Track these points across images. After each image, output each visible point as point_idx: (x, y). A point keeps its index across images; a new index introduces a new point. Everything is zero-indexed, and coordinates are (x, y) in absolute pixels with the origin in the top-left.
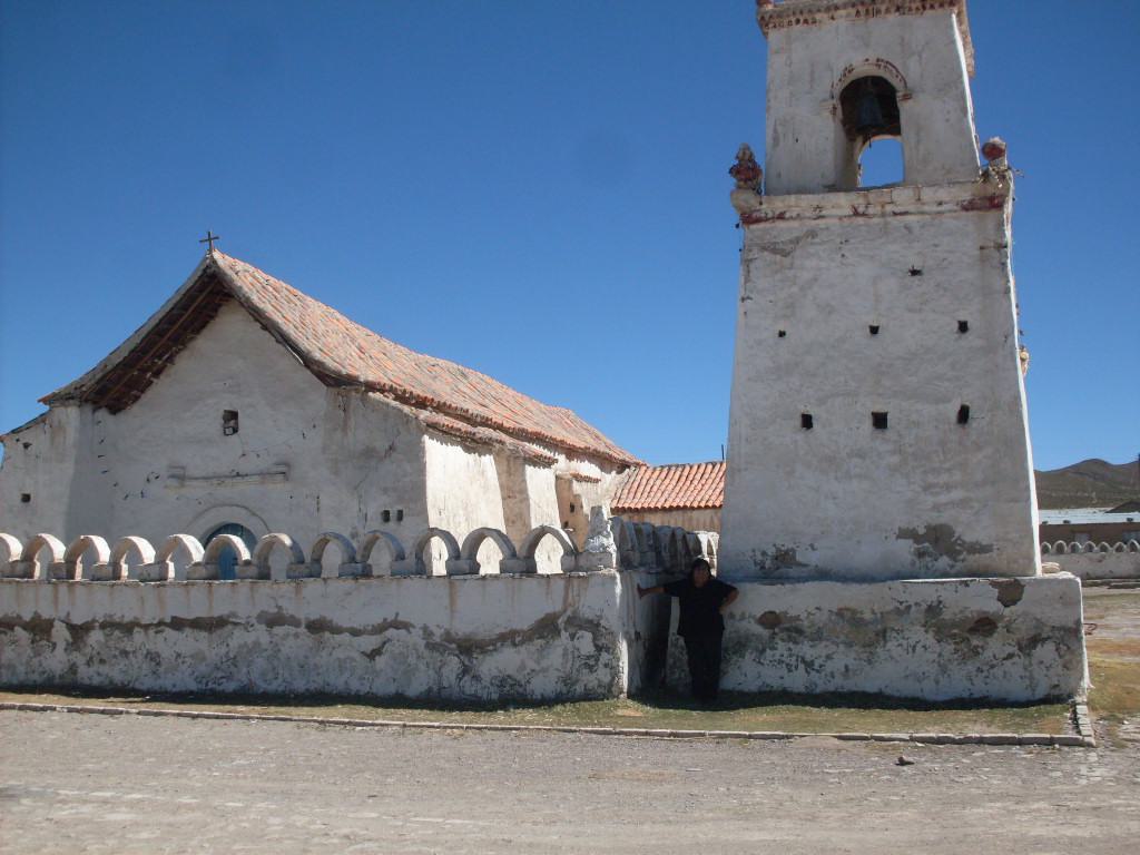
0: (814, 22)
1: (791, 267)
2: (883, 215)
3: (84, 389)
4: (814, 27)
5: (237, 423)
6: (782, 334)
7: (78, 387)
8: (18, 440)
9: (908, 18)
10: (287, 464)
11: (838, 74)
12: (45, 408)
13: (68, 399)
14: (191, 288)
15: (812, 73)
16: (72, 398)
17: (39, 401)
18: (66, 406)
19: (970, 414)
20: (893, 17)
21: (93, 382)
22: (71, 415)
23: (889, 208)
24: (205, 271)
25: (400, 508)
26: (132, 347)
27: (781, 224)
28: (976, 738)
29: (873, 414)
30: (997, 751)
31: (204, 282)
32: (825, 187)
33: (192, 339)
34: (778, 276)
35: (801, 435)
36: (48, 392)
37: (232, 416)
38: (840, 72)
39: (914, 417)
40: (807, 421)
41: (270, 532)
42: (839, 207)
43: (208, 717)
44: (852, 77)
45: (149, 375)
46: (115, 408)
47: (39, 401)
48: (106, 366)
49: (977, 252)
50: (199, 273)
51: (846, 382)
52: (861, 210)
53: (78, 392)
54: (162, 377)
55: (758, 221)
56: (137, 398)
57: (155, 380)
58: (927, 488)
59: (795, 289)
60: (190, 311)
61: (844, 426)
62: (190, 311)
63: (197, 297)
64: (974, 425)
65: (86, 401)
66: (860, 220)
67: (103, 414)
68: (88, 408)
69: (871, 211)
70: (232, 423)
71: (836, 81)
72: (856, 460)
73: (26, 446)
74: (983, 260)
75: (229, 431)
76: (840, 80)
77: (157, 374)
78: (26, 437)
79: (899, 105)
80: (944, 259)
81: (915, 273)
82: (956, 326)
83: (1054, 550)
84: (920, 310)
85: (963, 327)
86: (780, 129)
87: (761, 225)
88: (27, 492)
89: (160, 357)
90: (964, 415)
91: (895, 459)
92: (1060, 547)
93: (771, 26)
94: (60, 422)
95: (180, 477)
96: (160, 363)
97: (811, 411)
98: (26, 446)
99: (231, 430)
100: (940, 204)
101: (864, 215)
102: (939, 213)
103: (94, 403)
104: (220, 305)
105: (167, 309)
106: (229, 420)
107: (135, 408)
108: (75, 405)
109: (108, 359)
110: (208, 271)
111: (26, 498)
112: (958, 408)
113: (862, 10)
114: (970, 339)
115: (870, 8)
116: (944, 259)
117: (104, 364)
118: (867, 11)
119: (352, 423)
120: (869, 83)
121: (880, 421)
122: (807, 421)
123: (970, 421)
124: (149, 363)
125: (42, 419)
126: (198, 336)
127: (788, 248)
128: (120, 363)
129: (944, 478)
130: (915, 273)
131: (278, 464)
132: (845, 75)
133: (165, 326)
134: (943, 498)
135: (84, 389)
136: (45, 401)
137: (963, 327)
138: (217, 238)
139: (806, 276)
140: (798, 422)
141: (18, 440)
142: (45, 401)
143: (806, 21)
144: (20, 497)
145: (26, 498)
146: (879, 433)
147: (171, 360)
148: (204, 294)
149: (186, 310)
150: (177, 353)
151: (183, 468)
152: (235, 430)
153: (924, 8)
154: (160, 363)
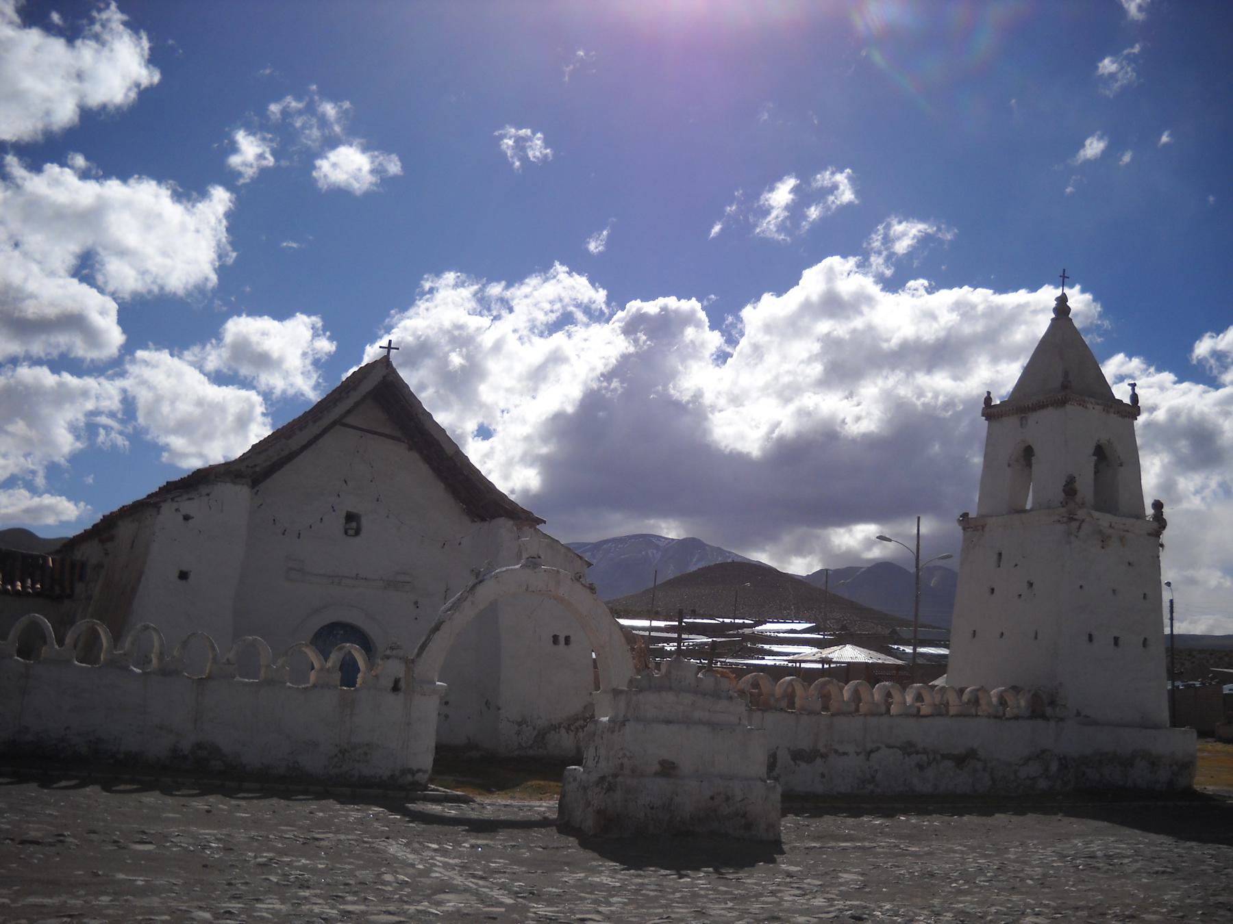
3: (257, 469)
8: (177, 510)
24: (384, 377)
73: (187, 518)
88: (185, 569)
111: (183, 576)
122: (1090, 638)
135: (257, 469)
141: (177, 510)
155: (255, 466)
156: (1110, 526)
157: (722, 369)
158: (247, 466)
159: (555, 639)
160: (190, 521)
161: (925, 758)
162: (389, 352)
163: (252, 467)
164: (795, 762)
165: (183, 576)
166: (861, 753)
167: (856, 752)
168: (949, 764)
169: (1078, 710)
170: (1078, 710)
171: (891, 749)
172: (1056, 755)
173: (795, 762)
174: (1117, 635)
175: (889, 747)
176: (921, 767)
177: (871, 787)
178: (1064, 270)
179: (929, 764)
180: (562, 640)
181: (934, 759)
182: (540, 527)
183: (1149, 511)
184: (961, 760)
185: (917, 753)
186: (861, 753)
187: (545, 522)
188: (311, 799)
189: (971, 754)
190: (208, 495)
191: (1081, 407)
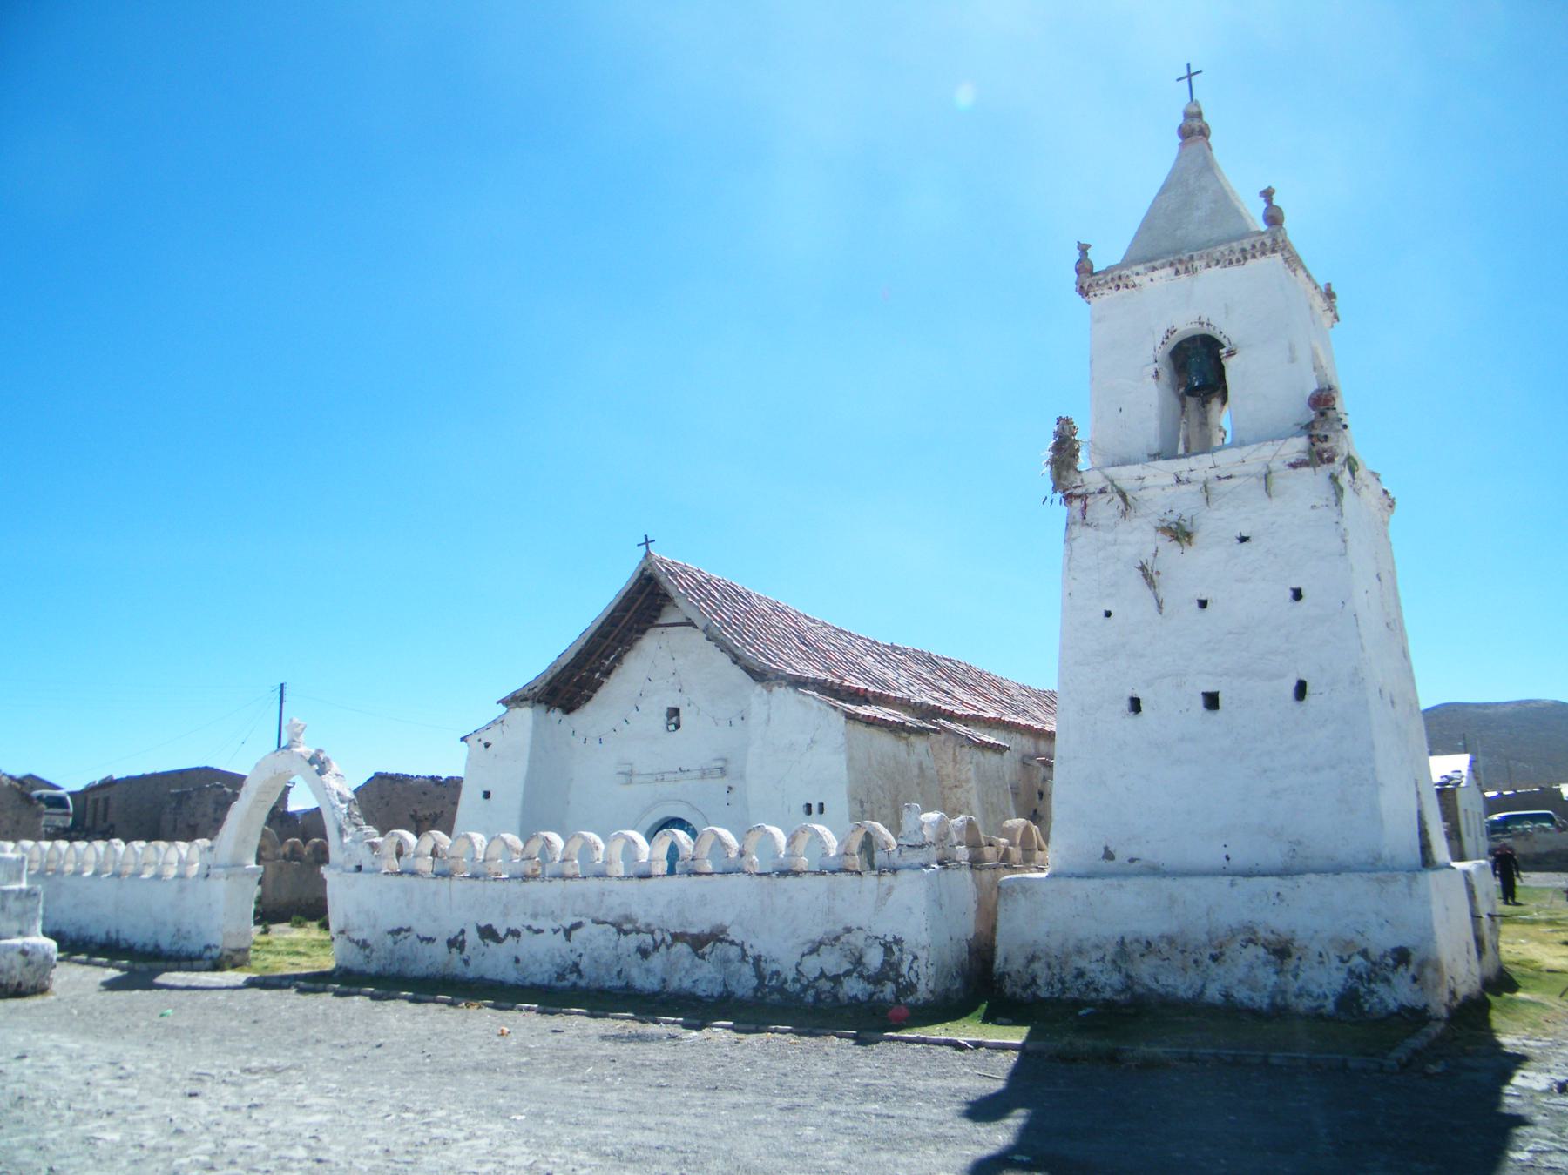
1: (1115, 543)
3: (536, 690)
5: (679, 720)
6: (1108, 614)
7: (530, 687)
8: (480, 740)
10: (725, 760)
11: (1159, 338)
12: (502, 709)
13: (522, 700)
14: (629, 591)
16: (526, 699)
17: (498, 703)
18: (520, 707)
19: (1308, 689)
21: (544, 683)
22: (525, 714)
24: (642, 573)
26: (578, 648)
29: (1203, 693)
30: (933, 1037)
31: (641, 584)
32: (1150, 456)
33: (637, 639)
34: (1101, 554)
35: (1131, 720)
36: (506, 693)
37: (674, 712)
38: (1163, 334)
40: (1136, 705)
41: (709, 825)
44: (1174, 340)
45: (598, 675)
46: (569, 709)
47: (498, 703)
51: (1174, 661)
52: (1183, 477)
53: (531, 693)
54: (612, 676)
56: (589, 698)
57: (605, 680)
60: (631, 612)
62: (631, 612)
63: (637, 599)
65: (539, 702)
66: (1183, 488)
67: (557, 714)
68: (541, 708)
70: (674, 720)
71: (1158, 344)
73: (487, 745)
75: (672, 727)
76: (1163, 343)
77: (607, 673)
79: (1223, 362)
80: (1272, 524)
82: (1289, 594)
88: (487, 789)
89: (607, 658)
90: (1301, 690)
93: (1091, 294)
95: (629, 776)
96: (607, 663)
99: (673, 726)
103: (546, 703)
104: (663, 606)
105: (609, 612)
106: (671, 718)
107: (589, 707)
108: (527, 705)
109: (557, 661)
110: (645, 573)
111: (487, 795)
112: (1294, 683)
113: (1181, 268)
115: (1190, 265)
116: (1272, 524)
117: (553, 666)
118: (1187, 268)
120: (1198, 343)
122: (1136, 705)
123: (1307, 697)
124: (597, 664)
125: (500, 721)
126: (644, 637)
128: (567, 665)
130: (1243, 540)
131: (715, 760)
132: (1167, 338)
133: (608, 628)
135: (536, 690)
136: (504, 702)
138: (654, 541)
140: (1126, 705)
142: (504, 702)
146: (1210, 714)
147: (619, 659)
148: (644, 595)
149: (628, 611)
150: (625, 652)
151: (631, 764)
152: (678, 727)
153: (1246, 259)
154: (607, 663)
155: (535, 688)
156: (1179, 481)
157: (1052, 436)
158: (529, 690)
161: (648, 938)
162: (647, 547)
163: (533, 689)
164: (484, 942)
165: (487, 795)
166: (558, 930)
167: (553, 930)
168: (683, 948)
169: (1106, 849)
170: (1106, 849)
171: (601, 926)
172: (877, 938)
173: (484, 942)
174: (1210, 689)
175: (597, 922)
176: (644, 953)
177: (573, 977)
178: (1200, 71)
179: (656, 948)
181: (663, 940)
184: (698, 943)
185: (638, 931)
186: (558, 930)
188: (790, 1031)
189: (716, 936)
191: (1123, 291)
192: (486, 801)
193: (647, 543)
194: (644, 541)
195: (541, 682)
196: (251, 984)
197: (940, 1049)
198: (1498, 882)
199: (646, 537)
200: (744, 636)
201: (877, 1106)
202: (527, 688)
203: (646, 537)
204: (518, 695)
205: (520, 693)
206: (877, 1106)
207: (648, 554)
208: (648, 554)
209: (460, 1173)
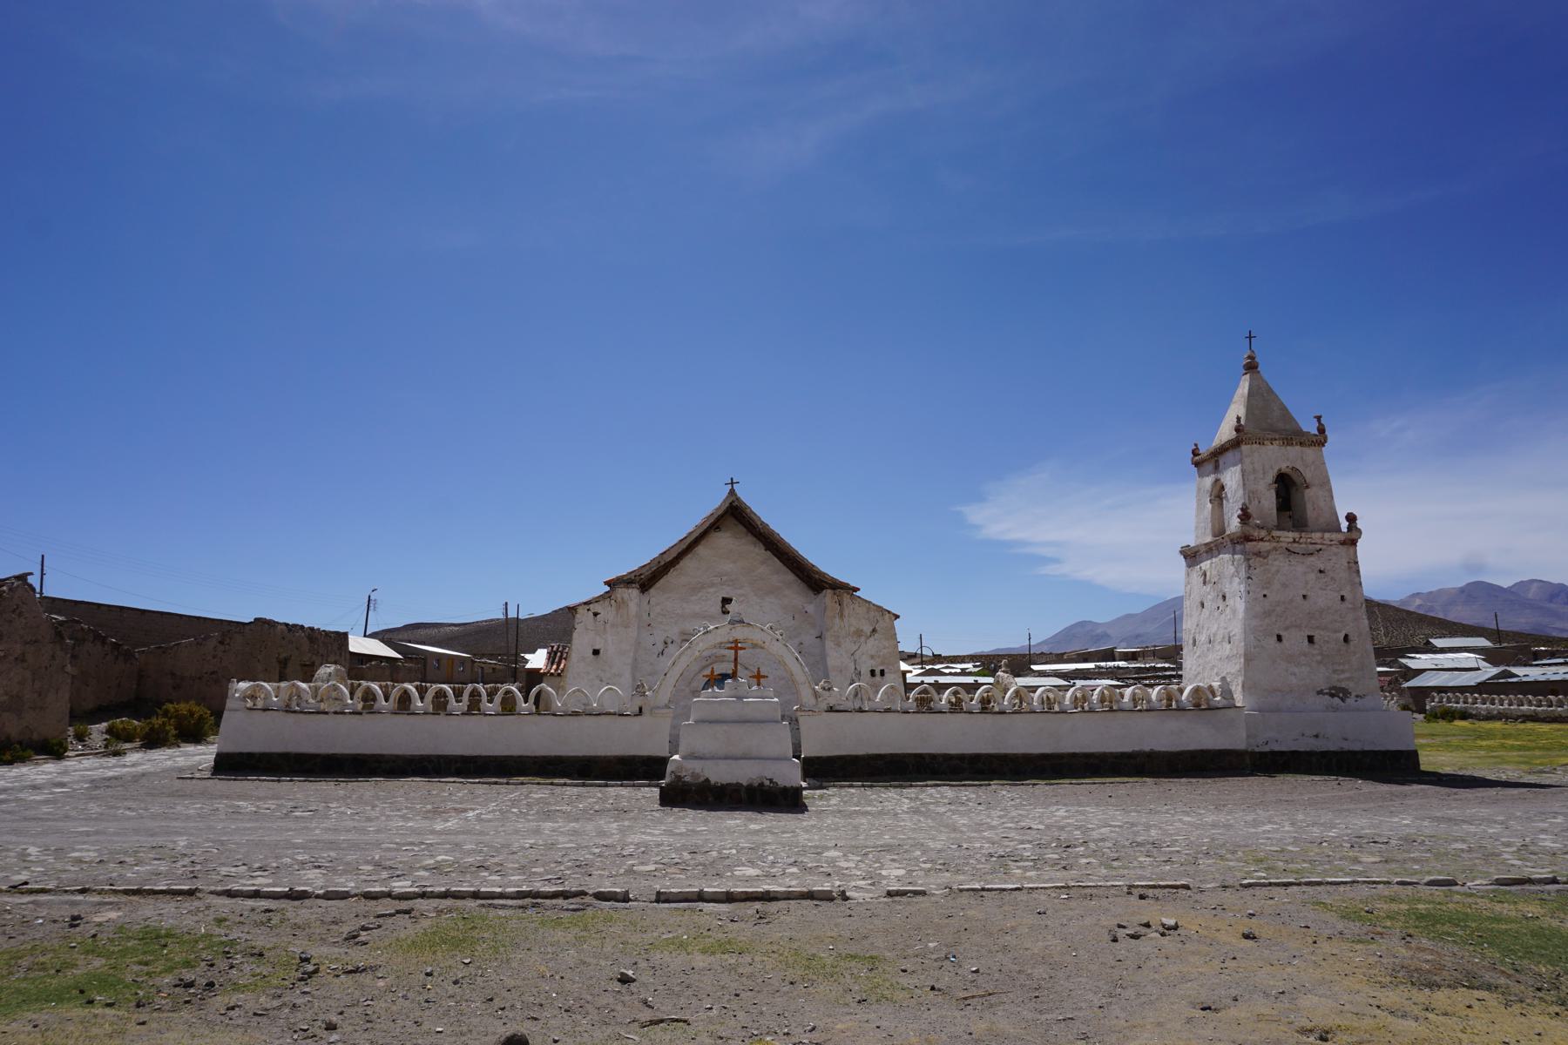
0: (1263, 444)
2: (1306, 543)
3: (642, 577)
4: (1262, 446)
6: (1265, 596)
8: (588, 610)
9: (1304, 448)
11: (1276, 471)
15: (1263, 469)
18: (628, 588)
20: (1298, 448)
23: (1309, 540)
24: (731, 503)
25: (882, 668)
27: (1261, 543)
28: (441, 892)
39: (1326, 639)
42: (1288, 537)
43: (1086, 784)
48: (659, 562)
49: (1346, 564)
50: (727, 505)
52: (1297, 540)
53: (638, 579)
55: (1251, 540)
58: (1335, 671)
59: (1270, 575)
61: (1294, 641)
64: (1352, 643)
69: (1301, 541)
72: (1303, 658)
73: (596, 614)
74: (1350, 568)
78: (595, 607)
81: (1321, 571)
83: (392, 704)
84: (1325, 590)
85: (1343, 598)
86: (1251, 495)
87: (1254, 543)
88: (597, 648)
90: (1346, 638)
91: (1319, 658)
92: (405, 699)
94: (622, 599)
97: (1281, 633)
98: (596, 614)
100: (1331, 541)
101: (1298, 542)
102: (1331, 545)
111: (596, 652)
114: (1347, 604)
119: (846, 612)
121: (1311, 639)
127: (1266, 554)
129: (1341, 667)
130: (1321, 571)
134: (1342, 676)
135: (642, 577)
136: (607, 583)
137: (1343, 598)
139: (1274, 569)
141: (588, 610)
142: (607, 583)
143: (1259, 443)
144: (591, 651)
145: (596, 652)
155: (641, 574)
159: (873, 673)
160: (598, 616)
180: (878, 672)
182: (858, 594)
183: (1344, 525)
187: (858, 589)
190: (610, 597)
192: (595, 657)
193: (732, 483)
194: (730, 481)
195: (647, 571)
196: (230, 765)
197: (1278, 888)
198: (1506, 582)
199: (732, 479)
200: (1526, 759)
201: (1491, 831)
202: (633, 574)
203: (732, 479)
204: (625, 578)
205: (628, 577)
206: (1491, 831)
207: (732, 492)
208: (732, 492)
209: (179, 1043)
